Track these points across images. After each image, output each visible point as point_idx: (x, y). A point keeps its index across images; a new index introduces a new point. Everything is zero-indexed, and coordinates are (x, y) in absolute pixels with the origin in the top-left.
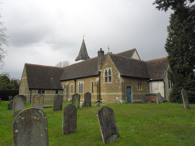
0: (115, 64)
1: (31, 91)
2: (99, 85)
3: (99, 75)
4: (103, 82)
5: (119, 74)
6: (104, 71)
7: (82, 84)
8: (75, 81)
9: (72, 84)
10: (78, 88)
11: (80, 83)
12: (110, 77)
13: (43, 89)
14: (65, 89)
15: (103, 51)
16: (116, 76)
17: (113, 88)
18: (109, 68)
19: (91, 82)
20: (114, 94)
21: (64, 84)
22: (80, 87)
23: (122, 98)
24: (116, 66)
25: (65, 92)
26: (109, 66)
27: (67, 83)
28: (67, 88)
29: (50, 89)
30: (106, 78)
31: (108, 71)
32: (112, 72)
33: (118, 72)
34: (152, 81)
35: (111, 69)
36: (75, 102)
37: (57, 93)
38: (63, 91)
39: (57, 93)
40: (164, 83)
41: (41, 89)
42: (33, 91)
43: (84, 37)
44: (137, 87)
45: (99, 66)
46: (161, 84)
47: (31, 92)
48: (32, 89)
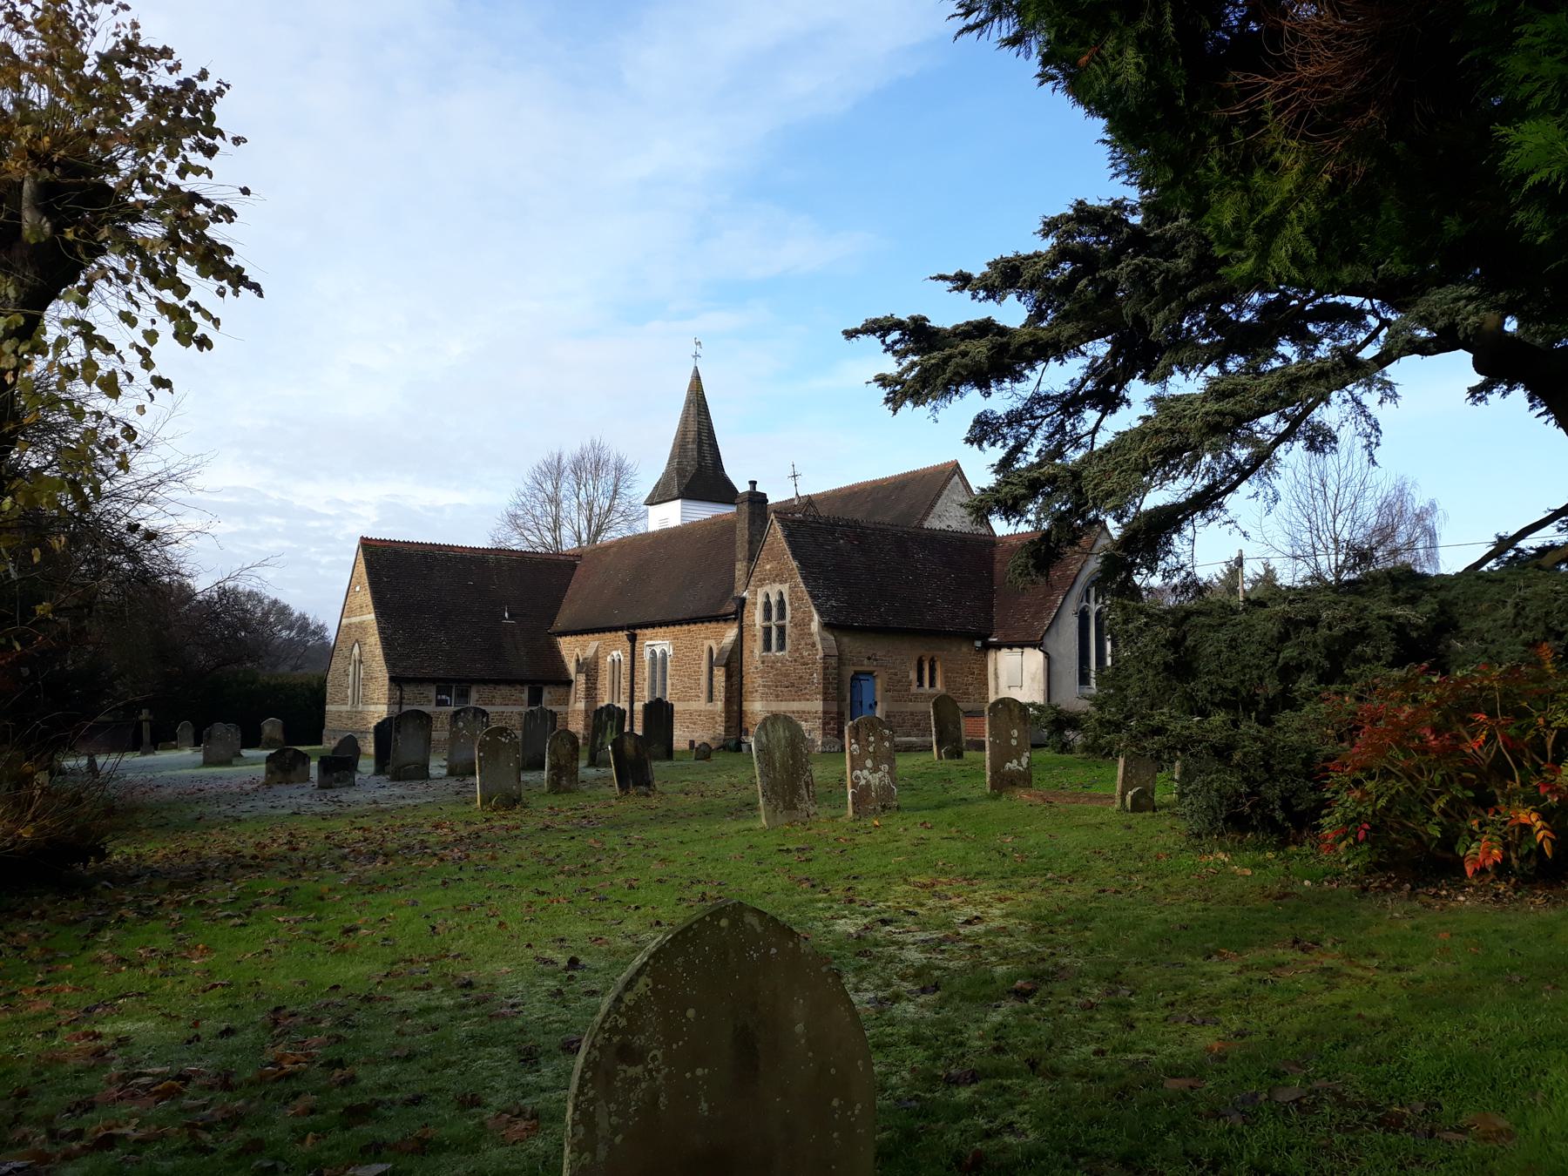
2: (732, 662)
3: (738, 613)
4: (754, 652)
5: (816, 617)
6: (760, 600)
7: (664, 654)
8: (633, 639)
9: (613, 650)
10: (644, 672)
11: (653, 653)
12: (781, 630)
13: (459, 681)
14: (582, 678)
15: (764, 495)
17: (793, 677)
18: (777, 587)
21: (572, 650)
22: (653, 672)
23: (825, 724)
24: (804, 578)
25: (581, 693)
26: (778, 577)
28: (590, 668)
29: (497, 682)
30: (767, 631)
31: (774, 599)
34: (998, 647)
35: (785, 588)
36: (604, 735)
37: (535, 698)
39: (535, 698)
40: (1048, 657)
41: (454, 681)
42: (409, 691)
43: (696, 356)
44: (913, 676)
45: (740, 568)
46: (1033, 660)
48: (409, 681)
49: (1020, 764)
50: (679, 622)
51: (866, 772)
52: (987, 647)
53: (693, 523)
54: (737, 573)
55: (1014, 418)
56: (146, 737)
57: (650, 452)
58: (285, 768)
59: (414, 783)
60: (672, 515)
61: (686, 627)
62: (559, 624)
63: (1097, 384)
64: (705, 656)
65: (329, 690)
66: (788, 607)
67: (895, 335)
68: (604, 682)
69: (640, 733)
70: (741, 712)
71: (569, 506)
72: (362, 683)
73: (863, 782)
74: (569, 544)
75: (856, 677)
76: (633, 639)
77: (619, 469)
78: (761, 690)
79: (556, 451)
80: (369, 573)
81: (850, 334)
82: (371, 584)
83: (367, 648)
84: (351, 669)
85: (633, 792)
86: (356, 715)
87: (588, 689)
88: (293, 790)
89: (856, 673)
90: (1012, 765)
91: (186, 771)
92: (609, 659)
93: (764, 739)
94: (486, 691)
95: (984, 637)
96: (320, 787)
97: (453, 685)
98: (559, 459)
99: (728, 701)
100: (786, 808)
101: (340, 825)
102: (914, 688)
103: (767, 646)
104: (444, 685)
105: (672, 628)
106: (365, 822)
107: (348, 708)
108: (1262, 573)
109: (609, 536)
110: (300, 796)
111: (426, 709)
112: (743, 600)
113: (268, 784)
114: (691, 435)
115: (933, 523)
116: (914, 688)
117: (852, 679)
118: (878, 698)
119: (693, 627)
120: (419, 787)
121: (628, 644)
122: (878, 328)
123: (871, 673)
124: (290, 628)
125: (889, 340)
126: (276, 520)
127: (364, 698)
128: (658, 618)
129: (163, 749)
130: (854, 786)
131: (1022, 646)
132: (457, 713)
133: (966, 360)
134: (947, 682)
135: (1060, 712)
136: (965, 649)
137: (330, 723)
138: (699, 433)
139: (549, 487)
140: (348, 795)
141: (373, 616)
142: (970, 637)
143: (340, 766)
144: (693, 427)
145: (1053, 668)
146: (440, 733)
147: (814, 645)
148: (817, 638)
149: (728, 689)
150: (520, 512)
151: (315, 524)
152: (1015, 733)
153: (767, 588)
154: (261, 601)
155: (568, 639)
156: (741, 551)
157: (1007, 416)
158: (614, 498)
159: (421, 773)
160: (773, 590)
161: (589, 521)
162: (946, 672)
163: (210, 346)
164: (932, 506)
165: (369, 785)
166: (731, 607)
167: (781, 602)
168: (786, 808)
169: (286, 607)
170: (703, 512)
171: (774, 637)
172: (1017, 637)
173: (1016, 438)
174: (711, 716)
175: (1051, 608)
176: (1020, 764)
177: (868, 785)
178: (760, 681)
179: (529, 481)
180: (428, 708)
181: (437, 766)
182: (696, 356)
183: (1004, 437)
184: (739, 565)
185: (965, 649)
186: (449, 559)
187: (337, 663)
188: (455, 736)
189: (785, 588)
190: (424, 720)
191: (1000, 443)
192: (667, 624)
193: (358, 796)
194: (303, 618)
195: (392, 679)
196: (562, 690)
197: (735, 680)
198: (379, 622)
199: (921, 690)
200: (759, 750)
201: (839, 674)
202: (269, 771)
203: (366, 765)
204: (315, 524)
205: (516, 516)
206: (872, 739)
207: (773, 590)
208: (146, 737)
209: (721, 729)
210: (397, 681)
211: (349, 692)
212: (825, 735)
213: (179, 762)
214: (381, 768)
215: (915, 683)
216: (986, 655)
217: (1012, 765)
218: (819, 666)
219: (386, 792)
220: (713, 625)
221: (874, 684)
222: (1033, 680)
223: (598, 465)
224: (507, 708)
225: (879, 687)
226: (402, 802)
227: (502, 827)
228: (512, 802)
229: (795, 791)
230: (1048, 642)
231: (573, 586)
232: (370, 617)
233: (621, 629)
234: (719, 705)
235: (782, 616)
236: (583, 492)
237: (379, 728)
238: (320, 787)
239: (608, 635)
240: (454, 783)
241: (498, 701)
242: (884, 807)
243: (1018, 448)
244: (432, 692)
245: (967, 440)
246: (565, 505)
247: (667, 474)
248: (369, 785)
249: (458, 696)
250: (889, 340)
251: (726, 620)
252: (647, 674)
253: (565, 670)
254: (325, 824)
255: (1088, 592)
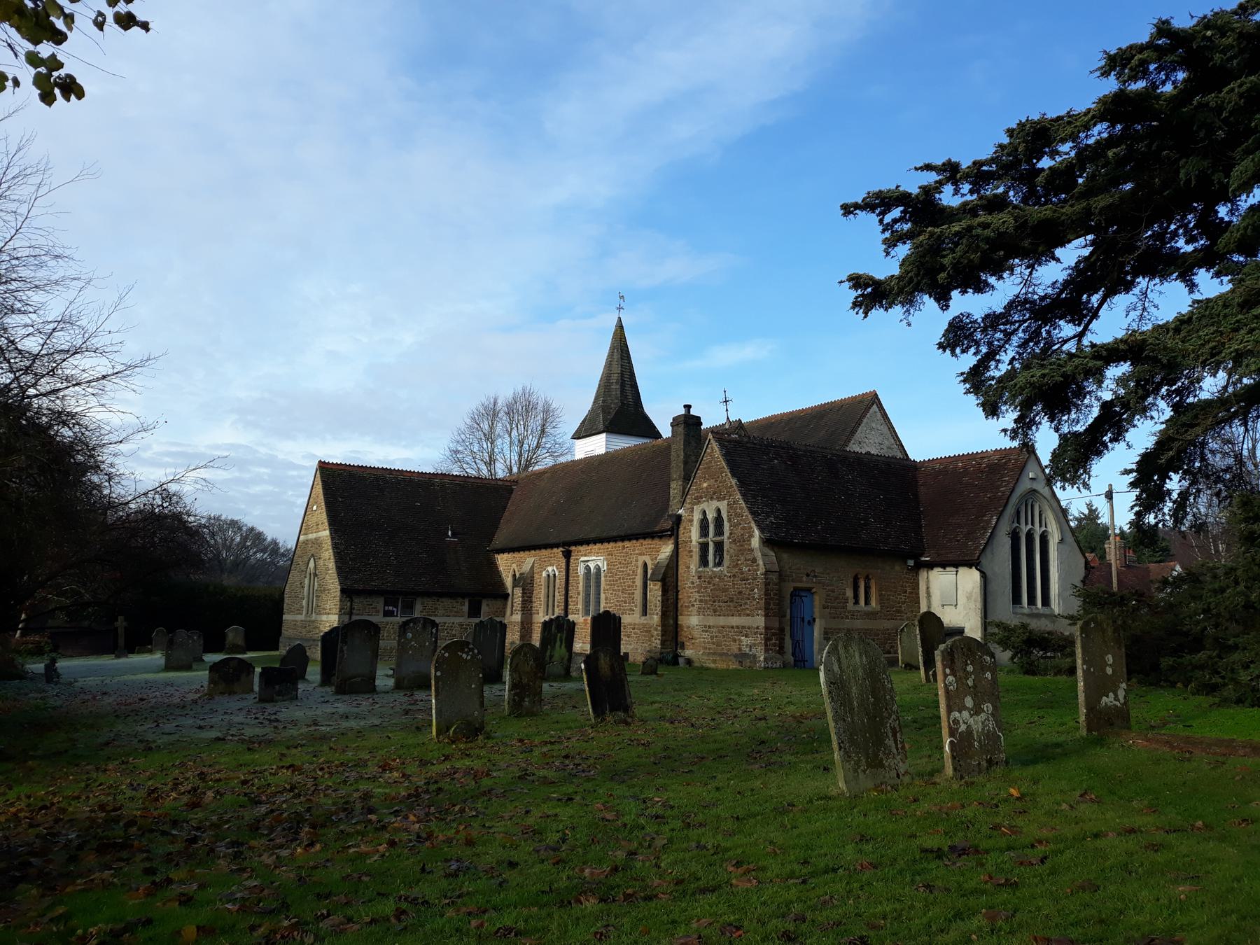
0: (742, 484)
1: (352, 601)
2: (669, 577)
3: (674, 530)
4: (690, 568)
5: (757, 533)
6: (697, 517)
7: (598, 569)
8: (567, 555)
9: (549, 566)
10: (579, 585)
11: (588, 568)
12: (719, 546)
16: (742, 541)
18: (715, 504)
19: (640, 564)
20: (735, 621)
22: (587, 586)
23: (767, 639)
24: (744, 495)
25: (518, 606)
26: (716, 495)
27: (527, 561)
28: (526, 583)
29: (440, 595)
30: (704, 548)
32: (729, 520)
33: (753, 525)
34: (930, 566)
35: (723, 506)
36: (553, 648)
37: (474, 611)
38: (505, 607)
39: (474, 611)
43: (620, 308)
44: (850, 593)
45: (675, 488)
46: (969, 579)
47: (352, 608)
48: (359, 593)
49: (1116, 699)
50: (614, 539)
51: (965, 714)
52: (920, 566)
53: (616, 451)
54: (672, 492)
55: (993, 321)
56: (121, 642)
57: (576, 397)
58: (229, 678)
59: (360, 698)
60: (597, 445)
61: (620, 544)
62: (498, 541)
63: (1071, 293)
64: (640, 571)
65: (286, 601)
66: (726, 523)
67: (896, 213)
68: (540, 594)
69: (537, 644)
70: (676, 624)
71: (503, 444)
72: (317, 593)
73: (963, 728)
74: (501, 472)
75: (796, 593)
76: (567, 555)
77: (547, 411)
78: (697, 604)
79: (492, 396)
80: (325, 494)
81: (848, 210)
82: (326, 503)
83: (321, 562)
84: (307, 581)
85: (609, 718)
86: (308, 624)
87: (524, 602)
88: (232, 703)
89: (796, 589)
90: (1108, 700)
91: (139, 677)
92: (544, 574)
93: (836, 668)
94: (430, 602)
95: (916, 557)
96: (262, 700)
97: (401, 597)
98: (495, 403)
99: (664, 615)
100: (869, 765)
101: (265, 758)
102: (850, 606)
103: (704, 561)
104: (391, 597)
105: (606, 545)
106: (298, 756)
107: (300, 617)
108: (1086, 512)
109: (545, 462)
110: (238, 713)
111: (374, 619)
112: (679, 517)
113: (210, 696)
114: (615, 377)
115: (854, 447)
116: (850, 606)
117: (792, 595)
118: (817, 615)
119: (627, 544)
120: (364, 702)
121: (564, 560)
122: (879, 202)
123: (809, 590)
124: (264, 551)
125: (888, 218)
126: (263, 470)
127: (319, 608)
128: (593, 535)
129: (139, 652)
130: (952, 733)
131: (956, 565)
132: (405, 624)
133: (987, 232)
134: (881, 599)
135: (1031, 632)
136: (897, 568)
137: (286, 631)
138: (622, 375)
139: (485, 426)
140: (287, 712)
141: (327, 532)
142: (903, 557)
143: (282, 681)
144: (617, 370)
145: (990, 588)
146: (388, 641)
147: (754, 560)
148: (758, 555)
149: (664, 603)
150: (460, 448)
151: (294, 473)
152: (1110, 659)
153: (704, 506)
154: (240, 528)
155: (505, 556)
156: (676, 471)
157: (984, 319)
158: (541, 437)
159: (367, 686)
160: (710, 508)
161: (520, 456)
162: (880, 590)
163: (80, 94)
164: (853, 432)
165: (314, 703)
166: (668, 524)
167: (719, 520)
168: (869, 765)
169: (260, 534)
170: (623, 443)
171: (711, 552)
172: (951, 557)
173: (990, 344)
174: (647, 630)
175: (985, 529)
176: (1116, 699)
177: (969, 731)
178: (697, 595)
179: (468, 421)
180: (377, 619)
181: (384, 680)
182: (620, 308)
183: (977, 343)
184: (673, 485)
185: (897, 568)
186: (399, 482)
187: (294, 577)
188: (402, 648)
189: (723, 506)
190: (373, 630)
191: (972, 350)
192: (601, 541)
193: (298, 714)
194: (275, 542)
195: (343, 591)
196: (499, 603)
197: (671, 594)
198: (332, 538)
199: (857, 608)
200: (830, 683)
201: (780, 590)
202: (211, 681)
203: (314, 672)
204: (294, 473)
205: (457, 452)
206: (970, 668)
207: (710, 508)
208: (121, 642)
209: (657, 643)
210: (347, 593)
211: (304, 602)
212: (767, 650)
213: (144, 667)
214: (326, 679)
215: (851, 601)
216: (917, 574)
217: (1108, 700)
218: (760, 581)
219: (329, 709)
220: (648, 541)
221: (812, 601)
222: (969, 598)
223: (529, 408)
224: (453, 621)
225: (817, 603)
226: (345, 724)
227: (468, 772)
228: (473, 731)
229: (879, 741)
230: (984, 562)
231: (510, 507)
232: (325, 533)
233: (557, 546)
234: (656, 619)
235: (719, 531)
236: (514, 433)
237: (323, 637)
238: (262, 700)
239: (544, 552)
240: (401, 697)
241: (441, 612)
242: (990, 762)
243: (992, 355)
244: (379, 603)
245: (941, 346)
246: (499, 442)
247: (593, 412)
248: (314, 703)
249: (403, 607)
250: (888, 218)
251: (661, 537)
252: (581, 589)
253: (501, 584)
254: (248, 757)
255: (1018, 513)
